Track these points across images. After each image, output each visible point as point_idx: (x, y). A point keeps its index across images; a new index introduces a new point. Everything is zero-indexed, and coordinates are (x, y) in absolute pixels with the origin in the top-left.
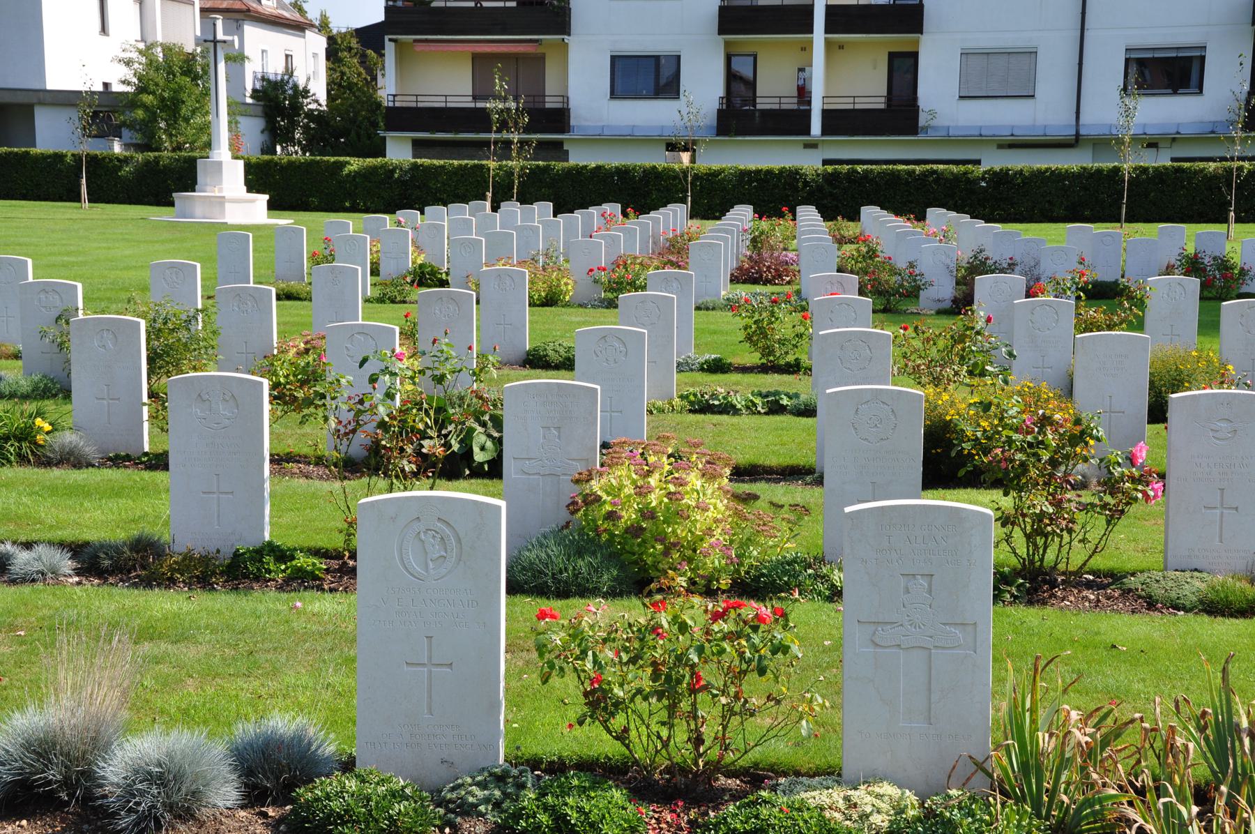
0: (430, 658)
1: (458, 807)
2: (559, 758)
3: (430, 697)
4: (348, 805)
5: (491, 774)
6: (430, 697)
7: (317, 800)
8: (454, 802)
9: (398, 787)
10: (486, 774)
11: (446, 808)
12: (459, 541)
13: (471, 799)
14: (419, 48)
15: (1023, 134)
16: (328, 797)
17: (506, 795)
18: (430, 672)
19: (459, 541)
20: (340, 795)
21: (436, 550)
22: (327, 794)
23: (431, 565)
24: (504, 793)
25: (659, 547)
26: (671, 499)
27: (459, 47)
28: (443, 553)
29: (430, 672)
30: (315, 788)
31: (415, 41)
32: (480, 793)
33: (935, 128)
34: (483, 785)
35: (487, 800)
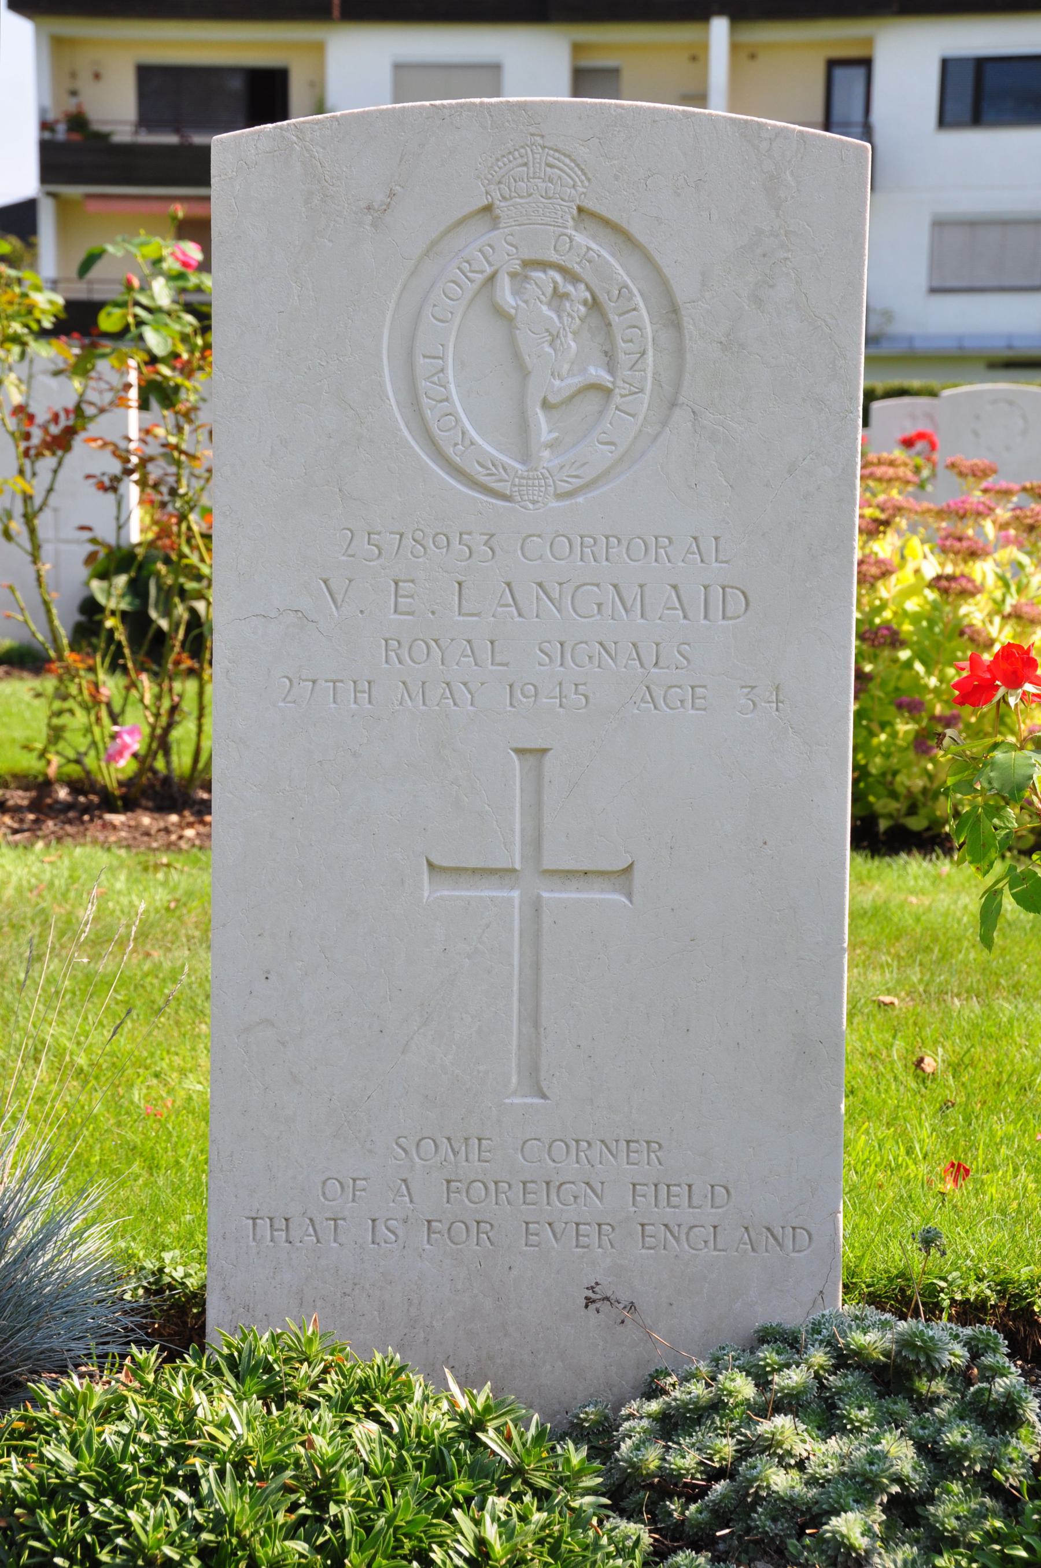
0: (535, 843)
1: (720, 1515)
2: (1002, 1288)
3: (533, 1017)
4: (220, 1522)
5: (844, 1360)
6: (533, 1017)
7: (55, 1493)
8: (694, 1494)
9: (439, 1420)
10: (819, 1357)
11: (656, 1520)
12: (672, 315)
13: (781, 1481)
14: (94, 206)
15: (1026, 348)
16: (111, 1481)
17: (941, 1461)
18: (535, 908)
19: (672, 315)
20: (174, 1464)
21: (565, 359)
22: (107, 1462)
23: (543, 427)
24: (927, 1450)
25: (905, 728)
26: (945, 592)
27: (155, 206)
28: (598, 373)
29: (535, 908)
30: (35, 1428)
31: (89, 196)
32: (826, 1453)
33: (892, 338)
34: (825, 1414)
35: (860, 1485)
